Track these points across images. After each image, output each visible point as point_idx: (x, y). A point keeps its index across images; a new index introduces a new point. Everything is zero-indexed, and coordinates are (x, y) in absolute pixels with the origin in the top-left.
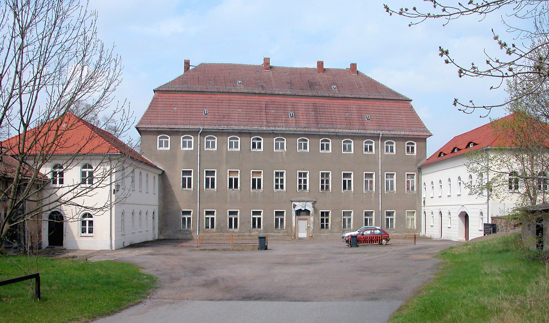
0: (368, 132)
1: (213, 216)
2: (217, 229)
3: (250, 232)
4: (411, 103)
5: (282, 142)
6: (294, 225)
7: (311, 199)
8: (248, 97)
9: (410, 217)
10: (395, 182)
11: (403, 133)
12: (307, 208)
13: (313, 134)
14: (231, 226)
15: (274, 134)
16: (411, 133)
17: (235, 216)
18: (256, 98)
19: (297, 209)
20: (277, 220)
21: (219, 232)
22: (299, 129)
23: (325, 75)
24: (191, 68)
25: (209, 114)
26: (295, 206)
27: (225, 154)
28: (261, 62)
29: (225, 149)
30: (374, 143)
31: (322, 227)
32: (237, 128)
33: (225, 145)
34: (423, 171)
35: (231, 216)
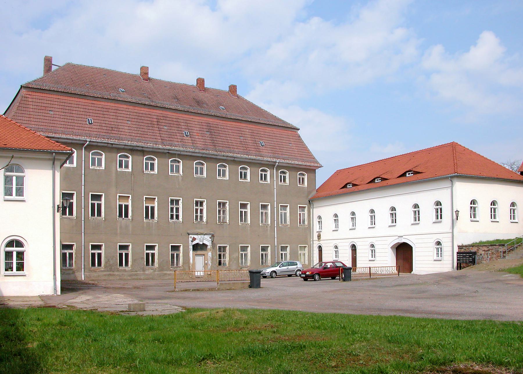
0: (265, 159)
1: (100, 251)
2: (105, 266)
3: (144, 271)
4: (299, 132)
5: (177, 164)
6: (191, 261)
7: (209, 232)
8: (137, 108)
9: (302, 252)
10: (288, 215)
11: (297, 162)
12: (205, 242)
13: (211, 158)
14: (121, 264)
15: (169, 154)
16: (304, 163)
17: (126, 251)
18: (145, 110)
19: (195, 242)
20: (173, 256)
21: (108, 271)
22: (197, 151)
23: (206, 94)
24: (54, 68)
25: (94, 124)
26: (194, 239)
27: (114, 175)
28: (137, 72)
29: (114, 169)
30: (269, 172)
31: (220, 263)
32: (129, 143)
33: (114, 164)
34: (316, 204)
35: (121, 251)
